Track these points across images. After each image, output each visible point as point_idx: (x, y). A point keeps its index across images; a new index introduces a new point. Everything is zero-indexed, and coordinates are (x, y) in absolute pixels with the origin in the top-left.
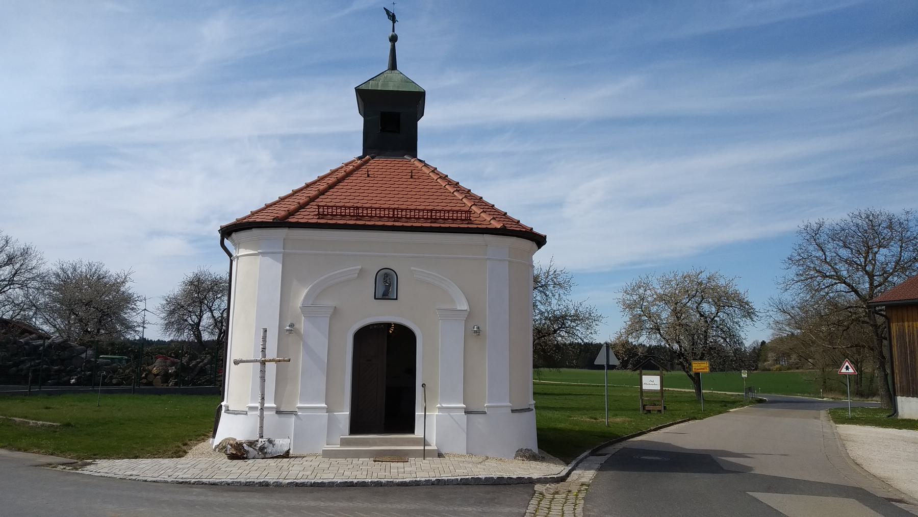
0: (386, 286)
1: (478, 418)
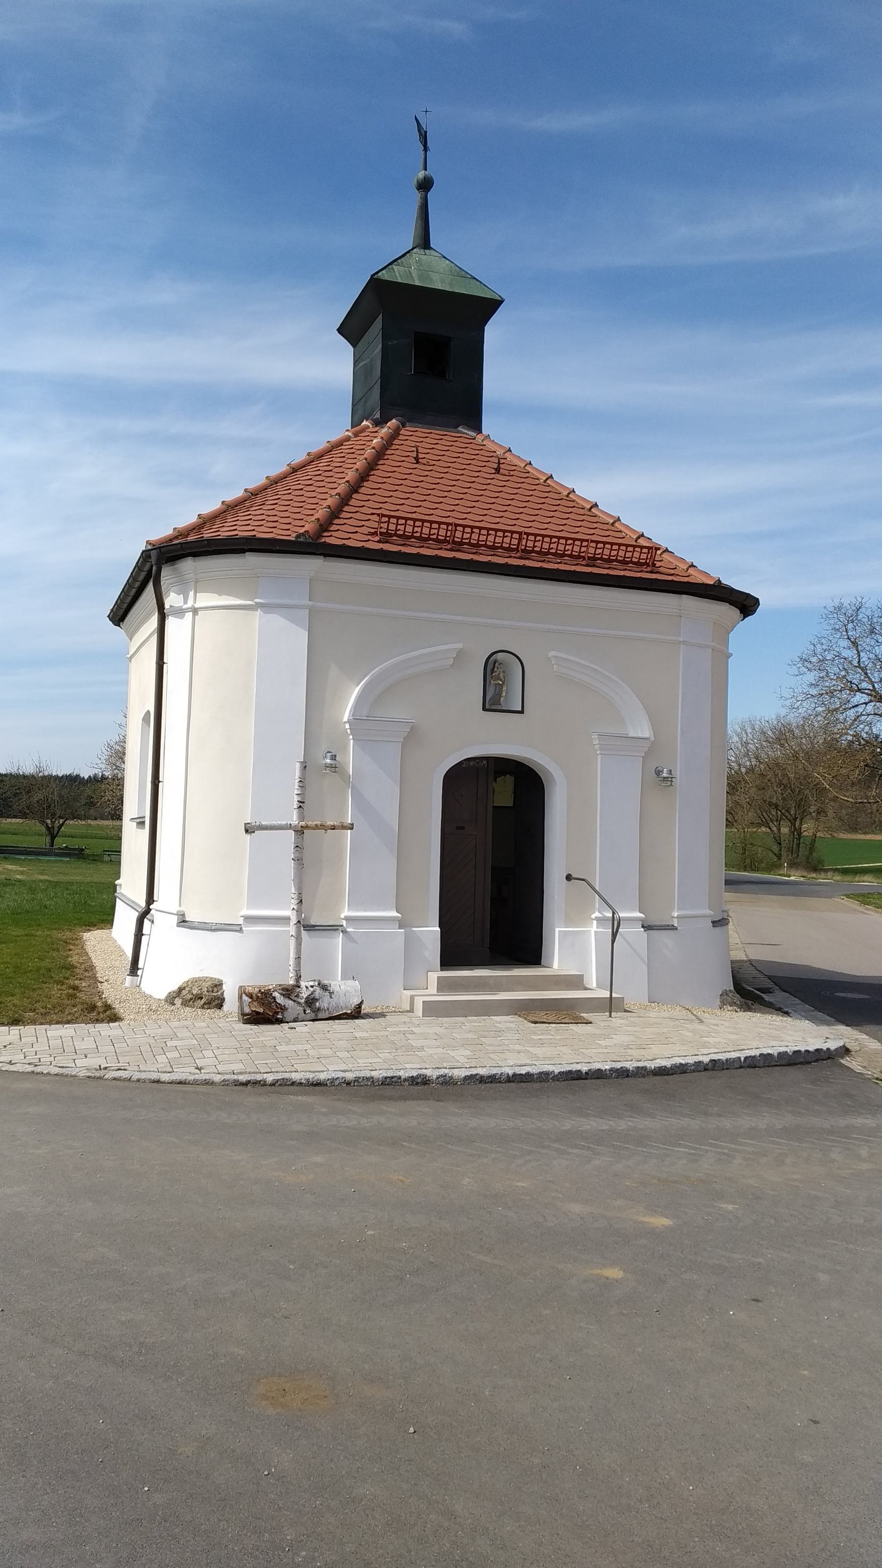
0: (497, 686)
1: (664, 937)
